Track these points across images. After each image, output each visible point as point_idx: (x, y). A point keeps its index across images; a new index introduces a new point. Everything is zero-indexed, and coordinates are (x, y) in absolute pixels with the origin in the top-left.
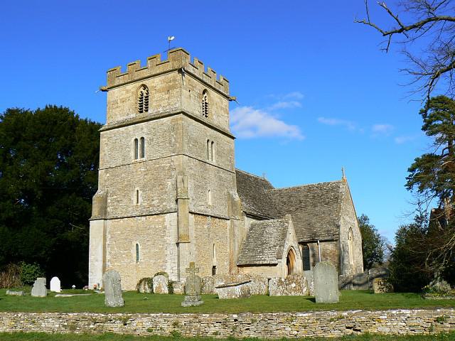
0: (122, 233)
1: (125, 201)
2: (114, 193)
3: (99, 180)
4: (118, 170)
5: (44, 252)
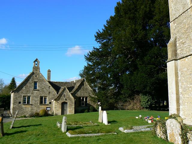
0: (188, 69)
1: (187, 42)
2: (180, 38)
3: (171, 30)
4: (181, 18)
5: (148, 88)
